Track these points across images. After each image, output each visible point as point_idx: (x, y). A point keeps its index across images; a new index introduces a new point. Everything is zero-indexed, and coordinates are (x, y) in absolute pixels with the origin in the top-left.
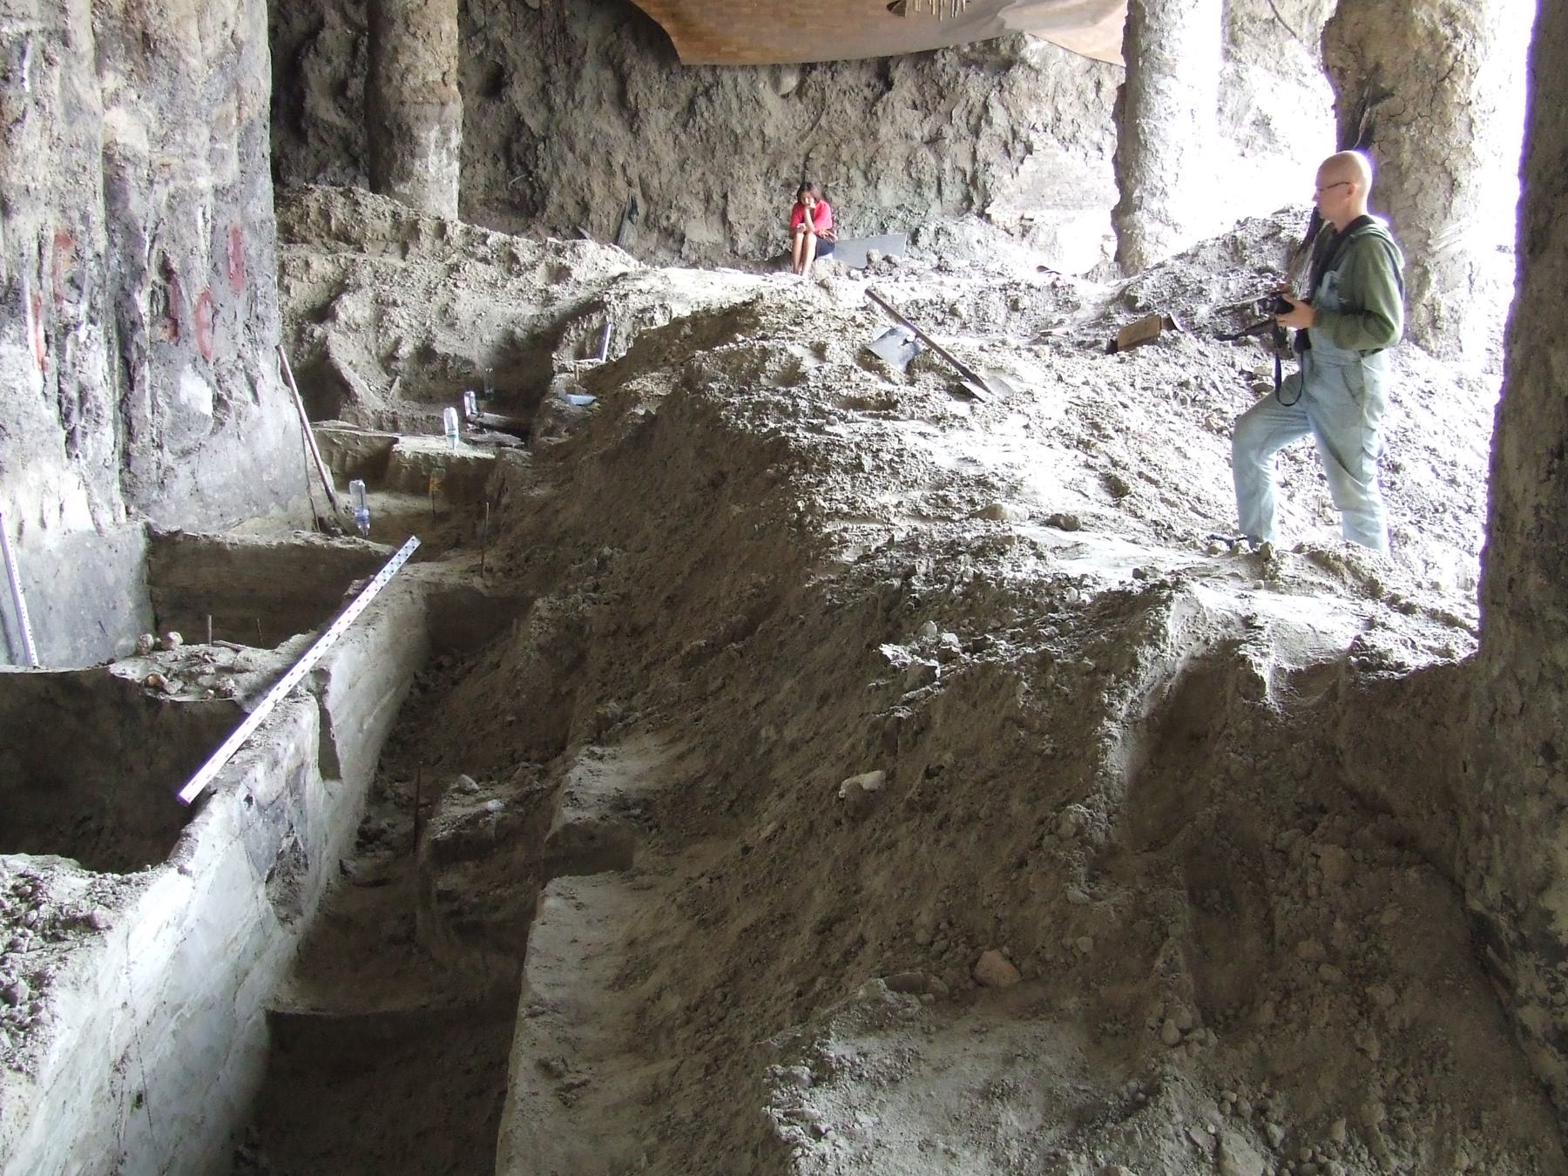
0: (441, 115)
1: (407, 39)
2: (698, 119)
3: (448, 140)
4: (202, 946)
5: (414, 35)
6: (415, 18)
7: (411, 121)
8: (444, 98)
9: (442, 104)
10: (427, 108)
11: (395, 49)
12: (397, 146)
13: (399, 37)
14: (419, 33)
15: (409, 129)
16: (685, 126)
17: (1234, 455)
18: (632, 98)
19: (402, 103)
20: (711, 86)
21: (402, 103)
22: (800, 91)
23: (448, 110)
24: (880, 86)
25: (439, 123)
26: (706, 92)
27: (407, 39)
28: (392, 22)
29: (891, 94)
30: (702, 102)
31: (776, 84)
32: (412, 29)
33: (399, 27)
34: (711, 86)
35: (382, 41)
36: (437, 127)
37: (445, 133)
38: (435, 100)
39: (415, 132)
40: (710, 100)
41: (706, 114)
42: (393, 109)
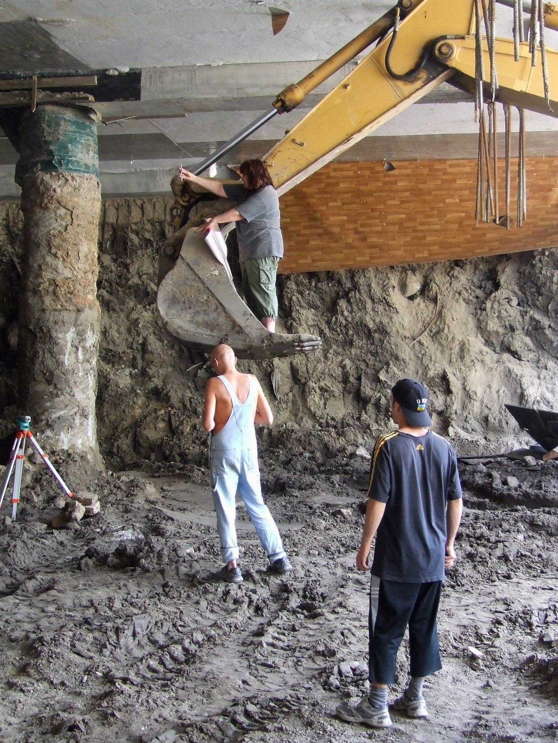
0: (76, 320)
1: (49, 259)
2: (340, 316)
3: (83, 340)
4: (547, 701)
5: (55, 256)
6: (56, 242)
7: (51, 324)
8: (80, 306)
9: (79, 311)
10: (65, 313)
11: (40, 266)
12: (39, 346)
13: (44, 257)
14: (59, 253)
15: (49, 331)
16: (328, 323)
17: (376, 545)
18: (287, 303)
19: (44, 310)
20: (350, 290)
21: (44, 310)
22: (425, 289)
23: (83, 316)
24: (489, 285)
25: (75, 325)
26: (346, 295)
27: (49, 259)
28: (38, 245)
29: (498, 294)
30: (343, 304)
31: (403, 287)
32: (54, 251)
33: (44, 250)
34: (350, 290)
35: (30, 261)
36: (73, 330)
37: (81, 335)
38: (72, 308)
39: (54, 334)
40: (349, 301)
41: (346, 313)
42: (37, 315)
